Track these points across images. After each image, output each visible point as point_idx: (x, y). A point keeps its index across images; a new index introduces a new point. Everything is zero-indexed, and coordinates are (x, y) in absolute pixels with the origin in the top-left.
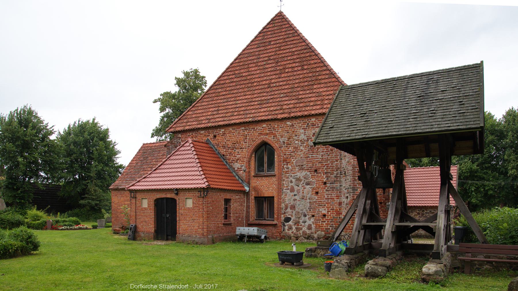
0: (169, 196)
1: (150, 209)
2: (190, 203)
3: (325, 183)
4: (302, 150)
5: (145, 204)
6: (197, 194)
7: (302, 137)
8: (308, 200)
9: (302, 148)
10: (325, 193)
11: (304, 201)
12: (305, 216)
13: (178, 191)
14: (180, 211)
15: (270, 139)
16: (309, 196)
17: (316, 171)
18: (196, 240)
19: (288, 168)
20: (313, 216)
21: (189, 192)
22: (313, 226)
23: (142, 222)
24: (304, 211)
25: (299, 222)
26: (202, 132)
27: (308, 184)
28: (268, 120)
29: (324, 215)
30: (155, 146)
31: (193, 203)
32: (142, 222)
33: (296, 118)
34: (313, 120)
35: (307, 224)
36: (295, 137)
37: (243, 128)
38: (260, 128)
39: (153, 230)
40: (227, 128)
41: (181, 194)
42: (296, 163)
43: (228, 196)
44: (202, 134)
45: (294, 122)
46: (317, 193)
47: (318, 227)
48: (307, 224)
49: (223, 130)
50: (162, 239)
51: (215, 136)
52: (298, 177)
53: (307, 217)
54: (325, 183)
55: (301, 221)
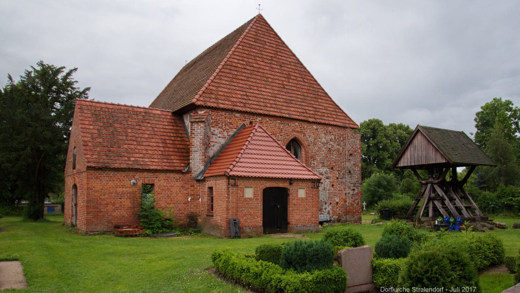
0: (281, 185)
1: (257, 199)
2: (302, 193)
3: (337, 178)
4: (323, 151)
5: (249, 193)
6: (310, 184)
7: (324, 140)
8: (328, 191)
9: (323, 149)
10: (338, 187)
11: (324, 191)
12: (326, 204)
13: (291, 181)
14: (292, 202)
15: (300, 136)
16: (328, 187)
17: (332, 168)
18: (311, 229)
19: (314, 164)
20: (331, 204)
21: (302, 182)
22: (331, 212)
23: (245, 215)
24: (325, 200)
25: (322, 209)
26: (238, 115)
27: (327, 178)
28: (300, 120)
29: (337, 203)
30: (107, 108)
31: (306, 193)
32: (245, 215)
33: (320, 124)
34: (330, 128)
35: (327, 210)
36: (319, 139)
37: (279, 122)
38: (293, 125)
39: (261, 223)
40: (264, 118)
41: (295, 184)
42: (320, 160)
43: (148, 178)
44: (237, 117)
45: (318, 127)
46: (333, 185)
47: (334, 212)
48: (327, 210)
49: (260, 119)
50: (275, 232)
51: (251, 123)
52: (321, 172)
53: (327, 205)
54: (337, 178)
55: (323, 208)
